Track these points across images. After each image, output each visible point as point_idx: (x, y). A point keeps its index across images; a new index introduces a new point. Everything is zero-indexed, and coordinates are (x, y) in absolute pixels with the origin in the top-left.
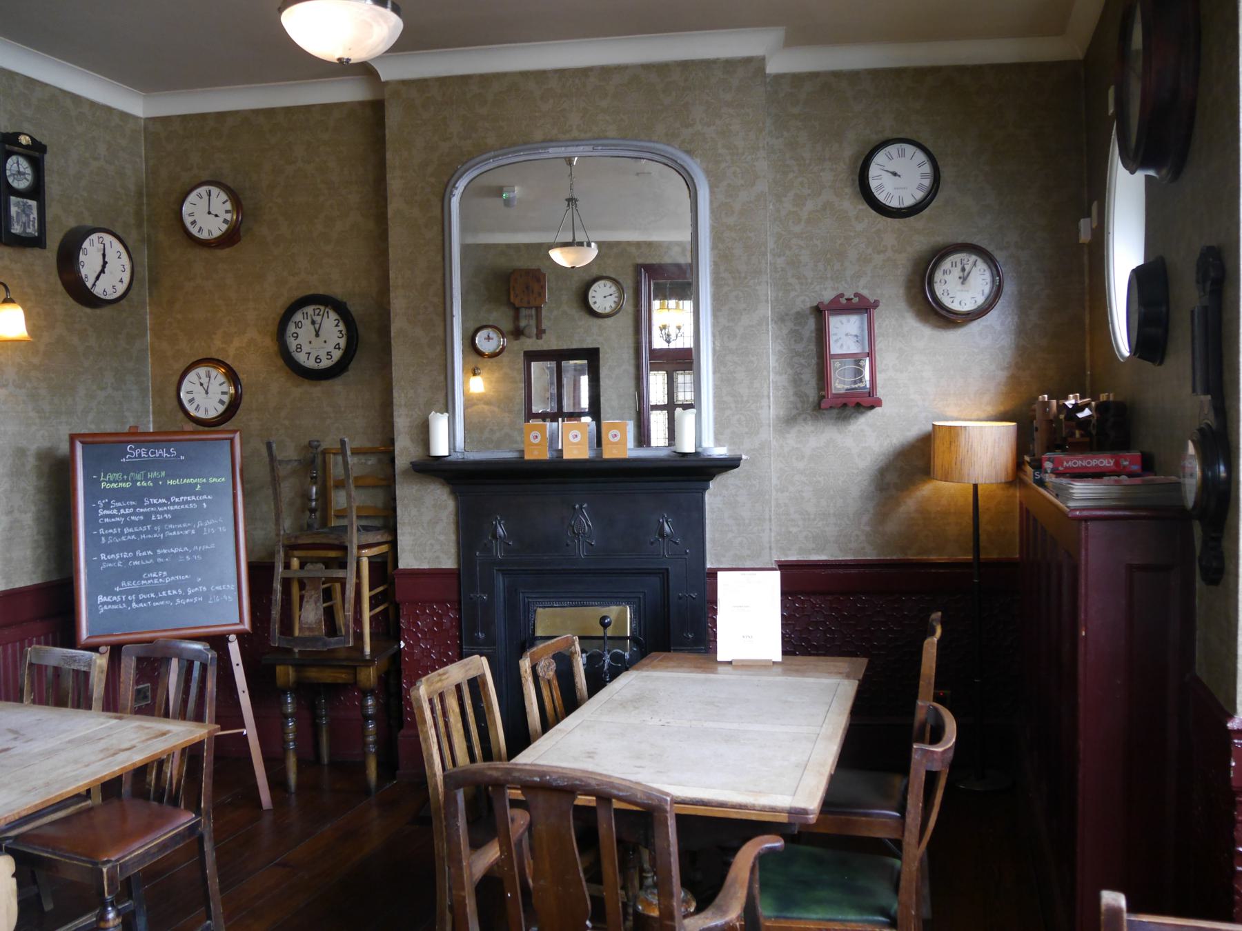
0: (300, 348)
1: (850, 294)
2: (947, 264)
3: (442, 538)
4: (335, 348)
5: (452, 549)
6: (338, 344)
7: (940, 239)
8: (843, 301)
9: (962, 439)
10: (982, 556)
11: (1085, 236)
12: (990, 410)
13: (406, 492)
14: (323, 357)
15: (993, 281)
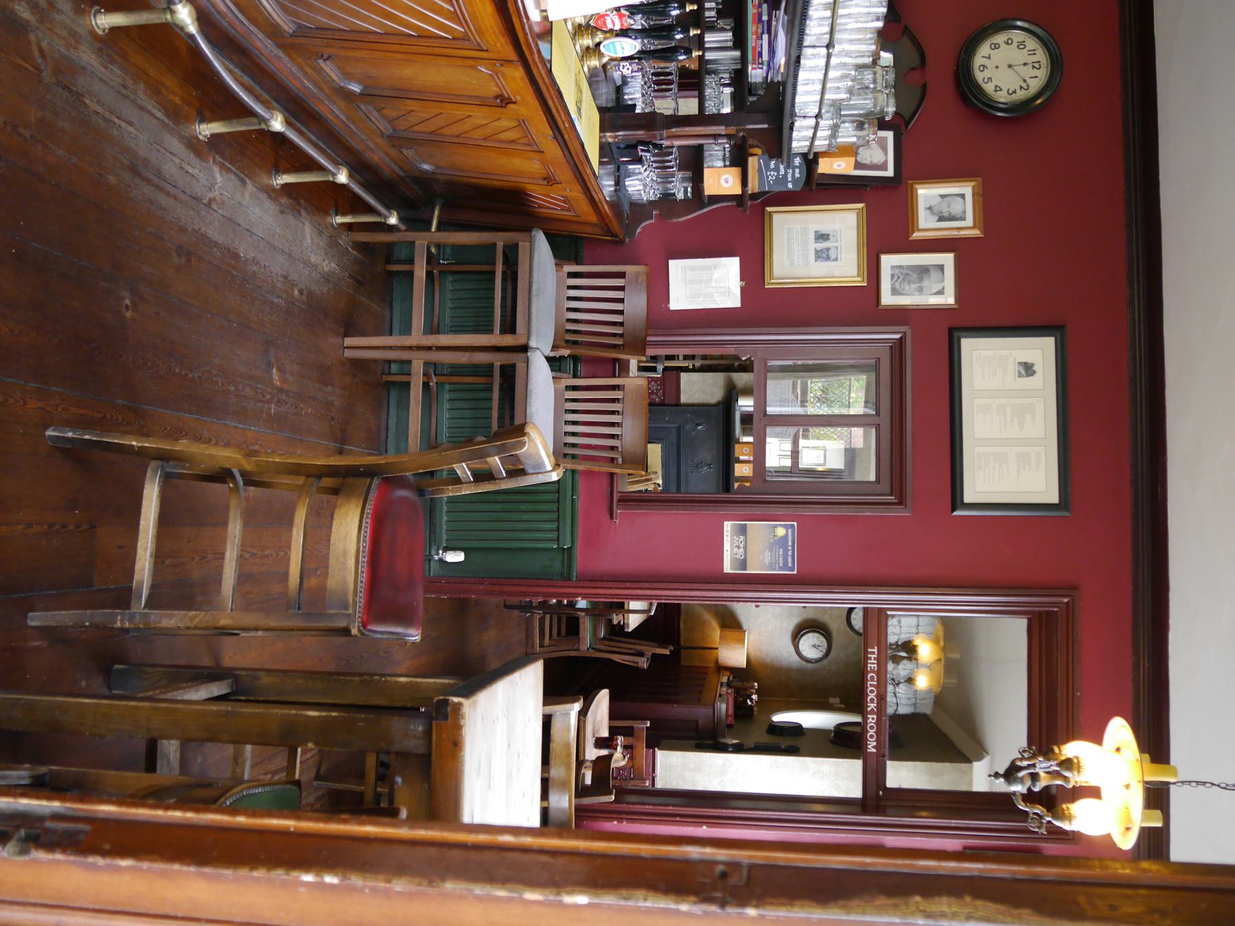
0: (995, 48)
2: (822, 639)
3: (696, 396)
4: (996, 86)
5: (690, 401)
6: (1001, 90)
7: (835, 635)
9: (738, 645)
10: (682, 650)
11: (832, 700)
12: (752, 655)
13: (719, 378)
14: (986, 74)
15: (813, 659)
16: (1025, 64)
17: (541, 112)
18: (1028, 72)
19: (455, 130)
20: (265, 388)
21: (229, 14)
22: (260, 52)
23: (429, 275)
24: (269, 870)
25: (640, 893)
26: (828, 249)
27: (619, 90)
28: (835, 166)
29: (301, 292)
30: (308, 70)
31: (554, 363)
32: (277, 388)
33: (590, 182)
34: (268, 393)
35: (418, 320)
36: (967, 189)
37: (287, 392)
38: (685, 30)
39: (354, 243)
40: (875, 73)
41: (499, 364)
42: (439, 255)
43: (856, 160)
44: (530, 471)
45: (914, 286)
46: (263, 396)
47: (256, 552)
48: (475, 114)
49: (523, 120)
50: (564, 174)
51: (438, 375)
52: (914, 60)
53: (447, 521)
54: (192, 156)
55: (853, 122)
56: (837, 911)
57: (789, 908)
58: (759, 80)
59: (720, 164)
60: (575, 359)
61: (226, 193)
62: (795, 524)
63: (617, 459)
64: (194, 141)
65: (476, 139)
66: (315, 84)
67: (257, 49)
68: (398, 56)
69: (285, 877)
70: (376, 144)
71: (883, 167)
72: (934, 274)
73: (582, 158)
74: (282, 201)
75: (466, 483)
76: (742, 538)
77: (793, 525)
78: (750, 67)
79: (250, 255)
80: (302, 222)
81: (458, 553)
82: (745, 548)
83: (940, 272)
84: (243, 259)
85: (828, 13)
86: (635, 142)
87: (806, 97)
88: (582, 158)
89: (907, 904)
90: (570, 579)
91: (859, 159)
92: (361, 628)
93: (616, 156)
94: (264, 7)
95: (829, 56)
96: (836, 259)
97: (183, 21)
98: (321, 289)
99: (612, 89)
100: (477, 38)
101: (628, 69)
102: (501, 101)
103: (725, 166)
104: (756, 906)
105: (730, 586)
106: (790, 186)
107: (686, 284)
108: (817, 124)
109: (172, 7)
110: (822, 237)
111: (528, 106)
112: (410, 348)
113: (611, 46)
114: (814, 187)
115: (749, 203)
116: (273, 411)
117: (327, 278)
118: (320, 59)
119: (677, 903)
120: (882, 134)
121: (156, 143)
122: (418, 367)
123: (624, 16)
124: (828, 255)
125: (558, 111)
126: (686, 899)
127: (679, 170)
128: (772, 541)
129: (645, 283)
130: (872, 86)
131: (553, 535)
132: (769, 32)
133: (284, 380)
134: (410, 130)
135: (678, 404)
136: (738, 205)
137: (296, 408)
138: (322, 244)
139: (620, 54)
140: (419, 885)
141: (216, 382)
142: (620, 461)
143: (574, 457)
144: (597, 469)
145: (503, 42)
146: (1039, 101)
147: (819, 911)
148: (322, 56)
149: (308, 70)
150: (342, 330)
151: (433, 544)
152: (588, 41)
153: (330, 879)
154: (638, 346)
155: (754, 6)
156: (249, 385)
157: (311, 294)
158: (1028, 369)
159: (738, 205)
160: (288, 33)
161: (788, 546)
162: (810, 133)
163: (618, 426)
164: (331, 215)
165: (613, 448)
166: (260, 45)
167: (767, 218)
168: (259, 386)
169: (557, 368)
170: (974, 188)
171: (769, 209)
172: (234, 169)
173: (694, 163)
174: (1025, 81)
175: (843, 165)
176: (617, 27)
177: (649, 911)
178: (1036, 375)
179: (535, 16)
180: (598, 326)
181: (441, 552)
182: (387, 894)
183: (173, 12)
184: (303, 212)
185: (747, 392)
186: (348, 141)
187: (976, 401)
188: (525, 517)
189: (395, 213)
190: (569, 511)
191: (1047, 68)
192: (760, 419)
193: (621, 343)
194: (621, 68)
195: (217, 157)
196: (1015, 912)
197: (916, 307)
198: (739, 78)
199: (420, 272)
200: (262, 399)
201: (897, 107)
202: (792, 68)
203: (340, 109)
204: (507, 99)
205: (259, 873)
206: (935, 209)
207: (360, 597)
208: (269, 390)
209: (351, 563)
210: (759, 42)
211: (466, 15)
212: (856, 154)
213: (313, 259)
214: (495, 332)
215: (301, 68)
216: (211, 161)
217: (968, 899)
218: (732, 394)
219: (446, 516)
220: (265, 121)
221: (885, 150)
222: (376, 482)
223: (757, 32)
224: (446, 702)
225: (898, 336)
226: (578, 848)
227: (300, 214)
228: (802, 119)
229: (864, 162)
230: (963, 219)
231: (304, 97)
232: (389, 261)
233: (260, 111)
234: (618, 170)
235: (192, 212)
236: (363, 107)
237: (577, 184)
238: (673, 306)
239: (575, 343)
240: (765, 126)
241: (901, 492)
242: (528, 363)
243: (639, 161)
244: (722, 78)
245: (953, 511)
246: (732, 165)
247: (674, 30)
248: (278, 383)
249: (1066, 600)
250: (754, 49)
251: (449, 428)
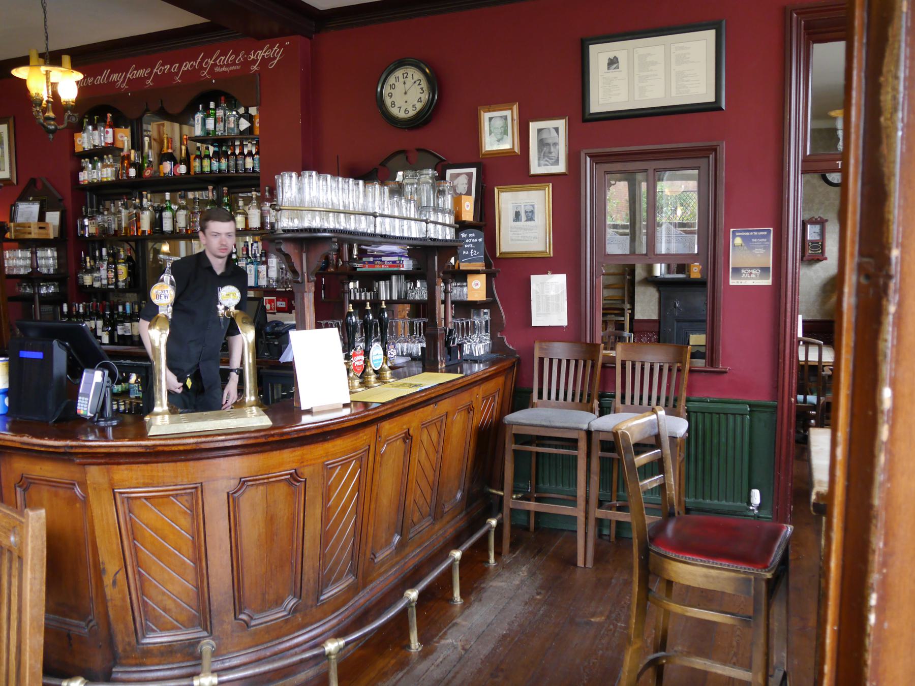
0: (394, 104)
1: (817, 217)
3: (653, 307)
4: (418, 101)
5: (656, 311)
6: (420, 98)
8: (814, 219)
14: (410, 109)
16: (404, 83)
17: (416, 412)
18: (409, 81)
19: (429, 472)
20: (605, 628)
21: (340, 618)
22: (368, 600)
23: (538, 500)
24: (866, 650)
25: (881, 345)
26: (526, 212)
27: (414, 359)
28: (468, 209)
29: (538, 594)
30: (382, 570)
31: (604, 411)
32: (606, 620)
33: (468, 380)
34: (609, 626)
35: (566, 510)
36: (486, 116)
37: (611, 612)
38: (382, 310)
39: (510, 552)
40: (407, 184)
41: (600, 452)
42: (524, 492)
43: (465, 194)
44: (656, 431)
45: (552, 149)
46: (611, 630)
47: (733, 652)
48: (417, 458)
49: (423, 425)
50: (465, 398)
51: (611, 499)
52: (401, 157)
53: (726, 501)
54: (431, 657)
55: (438, 197)
56: (892, 184)
57: (890, 223)
58: (411, 263)
59: (465, 289)
60: (601, 396)
61: (460, 638)
62: (732, 230)
63: (678, 367)
64: (422, 654)
65: (437, 458)
66: (393, 566)
67: (365, 603)
68: (373, 506)
69: (872, 638)
70: (440, 529)
71: (470, 175)
72: (544, 135)
73: (450, 385)
74: (473, 599)
75: (664, 480)
76: (743, 271)
77: (733, 232)
78: (402, 269)
79: (506, 626)
80: (489, 587)
81: (752, 494)
82: (751, 268)
83: (543, 131)
84: (508, 632)
85: (352, 217)
86: (446, 348)
87: (414, 231)
88: (450, 385)
89: (887, 128)
90: (776, 407)
91: (464, 193)
92: (767, 570)
93: (456, 362)
94: (336, 593)
95: (382, 216)
96: (533, 206)
97: (336, 648)
98: (539, 579)
99: (414, 363)
100: (360, 451)
101: (393, 351)
102: (408, 439)
103: (467, 286)
104: (890, 249)
105: (783, 280)
106: (480, 240)
107: (549, 314)
108: (432, 222)
109: (326, 653)
110: (517, 216)
111: (412, 420)
112: (586, 518)
113: (375, 363)
114: (483, 223)
115: (493, 269)
116: (623, 625)
117: (532, 574)
118: (374, 561)
119: (888, 314)
120: (448, 177)
121: (418, 681)
122: (601, 513)
123: (354, 353)
124: (530, 212)
125: (412, 400)
126: (884, 307)
127: (470, 318)
128: (745, 248)
129: (547, 344)
130: (415, 186)
131: (739, 418)
132: (381, 256)
133: (601, 614)
134: (429, 505)
135: (658, 322)
136: (495, 277)
137: (624, 607)
138: (507, 575)
139: (381, 356)
140: (876, 526)
141: (593, 663)
142: (679, 365)
143: (676, 400)
144: (685, 382)
145: (363, 434)
146: (427, 71)
147: (892, 199)
148: (372, 559)
149: (382, 570)
150: (572, 567)
151: (745, 514)
152: (372, 378)
153: (873, 600)
154: (591, 350)
155: (364, 267)
156: (600, 640)
157: (541, 587)
158: (613, 62)
159: (495, 277)
160: (354, 580)
161: (750, 235)
162: (439, 227)
163: (653, 365)
164: (489, 567)
165: (670, 370)
166: (362, 601)
167: (504, 256)
168: (602, 632)
169: (608, 410)
170: (485, 112)
171: (498, 254)
172: (445, 630)
173: (465, 308)
174: (415, 82)
175: (467, 203)
176: (363, 358)
177: (899, 338)
178: (617, 56)
179: (347, 412)
180: (578, 375)
181: (751, 508)
182: (888, 555)
183: (330, 654)
184: (482, 586)
185: (650, 269)
186: (436, 549)
187: (636, 98)
188: (723, 440)
189: (489, 520)
190: (720, 406)
191: (407, 68)
192: (650, 258)
193: (583, 362)
194: (392, 356)
195: (435, 640)
196: (891, 39)
197: (568, 146)
198: (410, 277)
199: (532, 506)
200: (612, 632)
201: (429, 168)
202: (389, 240)
203: (413, 551)
204: (406, 435)
205: (869, 659)
206: (499, 137)
207: (741, 568)
208: (606, 625)
209: (713, 572)
210: (386, 263)
211: (344, 458)
212: (461, 194)
213: (517, 582)
214: (576, 454)
215: (381, 575)
216: (437, 644)
217: (882, 79)
218: (652, 281)
219: (721, 501)
220: (410, 603)
221: (458, 175)
222: (653, 548)
223: (379, 265)
224: (816, 505)
225: (588, 159)
226: (848, 395)
227: (483, 588)
228: (428, 232)
229: (466, 189)
230: (506, 118)
231: (402, 575)
232: (527, 529)
233: (402, 605)
234: (466, 361)
235: (469, 663)
236: (411, 536)
237: (472, 389)
238: (564, 322)
239: (589, 395)
240: (436, 258)
241: (707, 150)
242: (600, 431)
243: (460, 346)
244: (410, 288)
245: (723, 110)
246: (466, 282)
247: (367, 319)
248: (603, 618)
249: (795, 15)
250: (390, 266)
251: (652, 494)
